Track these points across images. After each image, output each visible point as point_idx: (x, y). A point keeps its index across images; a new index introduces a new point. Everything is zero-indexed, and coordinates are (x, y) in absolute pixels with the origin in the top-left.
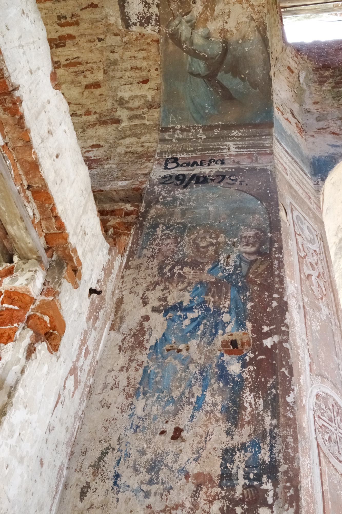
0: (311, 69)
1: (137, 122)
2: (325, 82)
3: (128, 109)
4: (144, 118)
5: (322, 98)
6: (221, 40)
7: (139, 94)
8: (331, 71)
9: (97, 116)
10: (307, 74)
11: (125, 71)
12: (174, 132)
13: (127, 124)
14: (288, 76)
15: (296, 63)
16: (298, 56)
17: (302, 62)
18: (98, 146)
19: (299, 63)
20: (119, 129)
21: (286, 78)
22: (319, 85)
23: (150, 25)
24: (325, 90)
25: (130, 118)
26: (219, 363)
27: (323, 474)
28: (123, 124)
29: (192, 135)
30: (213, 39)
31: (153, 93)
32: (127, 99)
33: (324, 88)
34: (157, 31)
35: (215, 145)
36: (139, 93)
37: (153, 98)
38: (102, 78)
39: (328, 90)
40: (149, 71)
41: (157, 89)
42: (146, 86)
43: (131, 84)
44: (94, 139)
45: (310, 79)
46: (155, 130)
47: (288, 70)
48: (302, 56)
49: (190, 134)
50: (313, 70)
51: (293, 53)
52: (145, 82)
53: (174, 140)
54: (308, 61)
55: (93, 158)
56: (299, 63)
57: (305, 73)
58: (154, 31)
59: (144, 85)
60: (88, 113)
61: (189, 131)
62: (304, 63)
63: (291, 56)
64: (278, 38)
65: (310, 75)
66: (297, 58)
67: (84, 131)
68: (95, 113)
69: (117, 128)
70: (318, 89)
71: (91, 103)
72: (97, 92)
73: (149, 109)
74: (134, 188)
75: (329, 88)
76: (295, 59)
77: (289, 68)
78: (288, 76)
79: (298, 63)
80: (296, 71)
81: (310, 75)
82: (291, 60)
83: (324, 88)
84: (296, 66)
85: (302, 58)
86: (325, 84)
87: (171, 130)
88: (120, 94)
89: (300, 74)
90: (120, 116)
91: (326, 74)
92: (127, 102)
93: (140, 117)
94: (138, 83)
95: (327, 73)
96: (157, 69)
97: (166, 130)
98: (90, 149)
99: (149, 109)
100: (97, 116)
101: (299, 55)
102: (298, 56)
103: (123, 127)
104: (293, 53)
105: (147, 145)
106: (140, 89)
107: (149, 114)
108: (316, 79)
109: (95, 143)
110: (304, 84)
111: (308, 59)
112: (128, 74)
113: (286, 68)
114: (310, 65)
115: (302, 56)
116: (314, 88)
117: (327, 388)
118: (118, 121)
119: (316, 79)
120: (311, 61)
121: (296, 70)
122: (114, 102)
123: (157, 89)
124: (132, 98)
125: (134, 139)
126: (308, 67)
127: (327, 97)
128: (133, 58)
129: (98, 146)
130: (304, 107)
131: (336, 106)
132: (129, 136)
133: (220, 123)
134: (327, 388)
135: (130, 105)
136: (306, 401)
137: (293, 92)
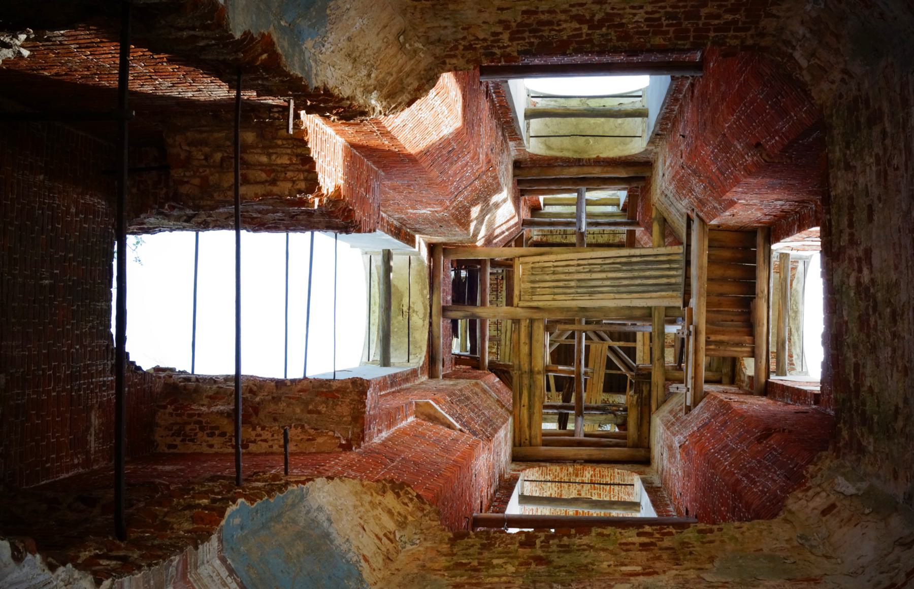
0: (835, 462)
2: (860, 444)
5: (887, 459)
8: (841, 425)
10: (843, 475)
14: (838, 519)
15: (819, 493)
16: (808, 485)
17: (818, 480)
19: (819, 486)
21: (841, 527)
22: (864, 456)
24: (874, 447)
26: (157, 481)
33: (871, 448)
39: (875, 442)
45: (853, 468)
47: (828, 516)
48: (808, 476)
50: (837, 457)
51: (800, 495)
54: (820, 465)
56: (819, 486)
57: (839, 478)
62: (822, 476)
63: (803, 502)
64: (764, 533)
65: (844, 467)
66: (810, 488)
70: (872, 459)
75: (871, 440)
76: (810, 493)
77: (824, 513)
78: (838, 519)
79: (819, 489)
80: (833, 498)
81: (844, 467)
82: (812, 505)
83: (871, 448)
84: (823, 494)
85: (812, 477)
86: (864, 444)
89: (838, 489)
91: (847, 437)
95: (845, 434)
101: (806, 482)
102: (808, 485)
104: (800, 495)
108: (854, 457)
110: (859, 484)
111: (816, 465)
113: (824, 519)
114: (828, 461)
115: (808, 476)
116: (870, 468)
119: (854, 457)
120: (820, 458)
121: (832, 496)
126: (829, 469)
127: (887, 450)
130: (901, 501)
131: (904, 439)
137: (869, 518)
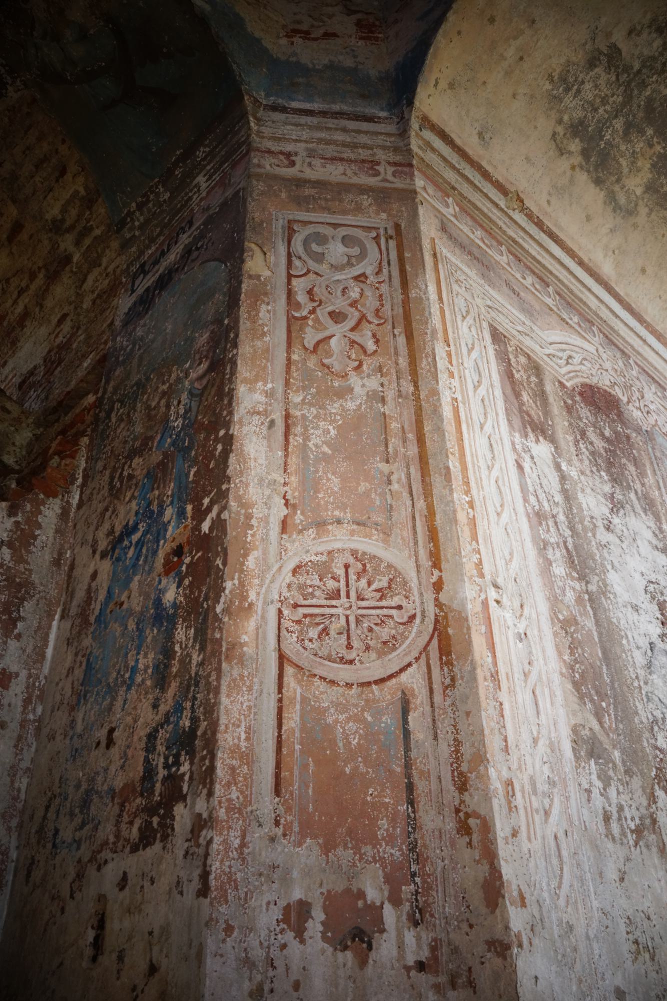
1: (87, 242)
3: (68, 230)
4: (91, 229)
6: (102, 24)
7: (68, 197)
9: (43, 271)
11: (32, 177)
12: (132, 219)
13: (78, 255)
18: (64, 317)
20: (74, 270)
23: (8, 86)
25: (78, 243)
27: (285, 702)
28: (76, 258)
29: (154, 205)
30: (92, 32)
31: (81, 180)
32: (60, 217)
34: (22, 87)
35: (183, 198)
36: (66, 195)
37: (86, 188)
38: (16, 212)
40: (57, 152)
41: (83, 171)
42: (68, 177)
43: (51, 190)
44: (57, 310)
46: (111, 236)
49: (150, 205)
52: (63, 172)
53: (137, 233)
55: (65, 340)
58: (19, 90)
59: (65, 177)
60: (33, 276)
61: (148, 201)
67: (42, 306)
68: (39, 268)
69: (72, 271)
71: (28, 259)
72: (24, 236)
73: (90, 208)
74: (99, 360)
87: (129, 220)
88: (48, 217)
90: (66, 250)
92: (63, 221)
93: (88, 230)
94: (57, 181)
96: (63, 142)
97: (122, 224)
98: (58, 330)
99: (90, 208)
100: (43, 271)
103: (77, 263)
105: (110, 269)
106: (64, 188)
107: (94, 216)
109: (59, 316)
112: (37, 179)
117: (331, 541)
118: (68, 259)
122: (50, 235)
123: (83, 171)
124: (64, 210)
125: (96, 272)
128: (27, 152)
129: (64, 317)
132: (88, 272)
133: (178, 153)
134: (331, 541)
135: (68, 223)
136: (258, 594)
